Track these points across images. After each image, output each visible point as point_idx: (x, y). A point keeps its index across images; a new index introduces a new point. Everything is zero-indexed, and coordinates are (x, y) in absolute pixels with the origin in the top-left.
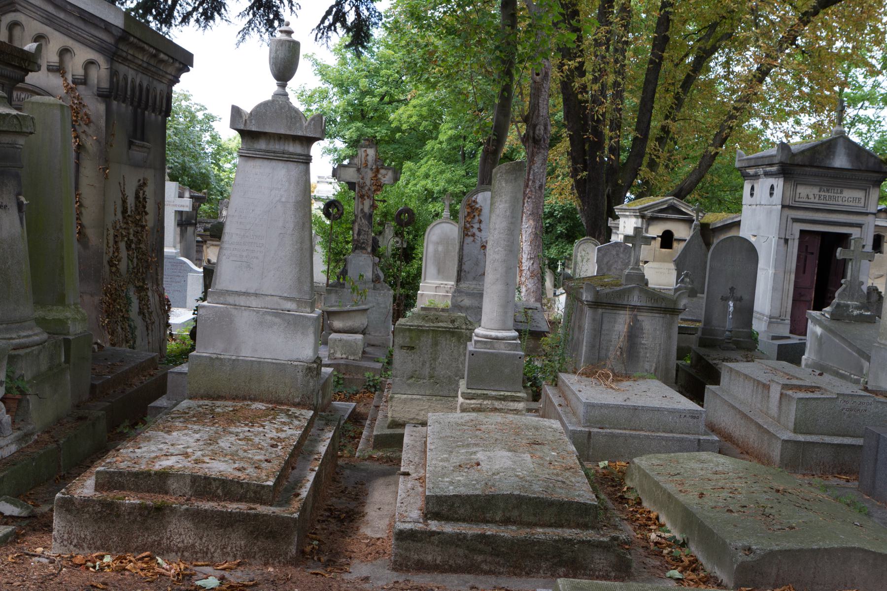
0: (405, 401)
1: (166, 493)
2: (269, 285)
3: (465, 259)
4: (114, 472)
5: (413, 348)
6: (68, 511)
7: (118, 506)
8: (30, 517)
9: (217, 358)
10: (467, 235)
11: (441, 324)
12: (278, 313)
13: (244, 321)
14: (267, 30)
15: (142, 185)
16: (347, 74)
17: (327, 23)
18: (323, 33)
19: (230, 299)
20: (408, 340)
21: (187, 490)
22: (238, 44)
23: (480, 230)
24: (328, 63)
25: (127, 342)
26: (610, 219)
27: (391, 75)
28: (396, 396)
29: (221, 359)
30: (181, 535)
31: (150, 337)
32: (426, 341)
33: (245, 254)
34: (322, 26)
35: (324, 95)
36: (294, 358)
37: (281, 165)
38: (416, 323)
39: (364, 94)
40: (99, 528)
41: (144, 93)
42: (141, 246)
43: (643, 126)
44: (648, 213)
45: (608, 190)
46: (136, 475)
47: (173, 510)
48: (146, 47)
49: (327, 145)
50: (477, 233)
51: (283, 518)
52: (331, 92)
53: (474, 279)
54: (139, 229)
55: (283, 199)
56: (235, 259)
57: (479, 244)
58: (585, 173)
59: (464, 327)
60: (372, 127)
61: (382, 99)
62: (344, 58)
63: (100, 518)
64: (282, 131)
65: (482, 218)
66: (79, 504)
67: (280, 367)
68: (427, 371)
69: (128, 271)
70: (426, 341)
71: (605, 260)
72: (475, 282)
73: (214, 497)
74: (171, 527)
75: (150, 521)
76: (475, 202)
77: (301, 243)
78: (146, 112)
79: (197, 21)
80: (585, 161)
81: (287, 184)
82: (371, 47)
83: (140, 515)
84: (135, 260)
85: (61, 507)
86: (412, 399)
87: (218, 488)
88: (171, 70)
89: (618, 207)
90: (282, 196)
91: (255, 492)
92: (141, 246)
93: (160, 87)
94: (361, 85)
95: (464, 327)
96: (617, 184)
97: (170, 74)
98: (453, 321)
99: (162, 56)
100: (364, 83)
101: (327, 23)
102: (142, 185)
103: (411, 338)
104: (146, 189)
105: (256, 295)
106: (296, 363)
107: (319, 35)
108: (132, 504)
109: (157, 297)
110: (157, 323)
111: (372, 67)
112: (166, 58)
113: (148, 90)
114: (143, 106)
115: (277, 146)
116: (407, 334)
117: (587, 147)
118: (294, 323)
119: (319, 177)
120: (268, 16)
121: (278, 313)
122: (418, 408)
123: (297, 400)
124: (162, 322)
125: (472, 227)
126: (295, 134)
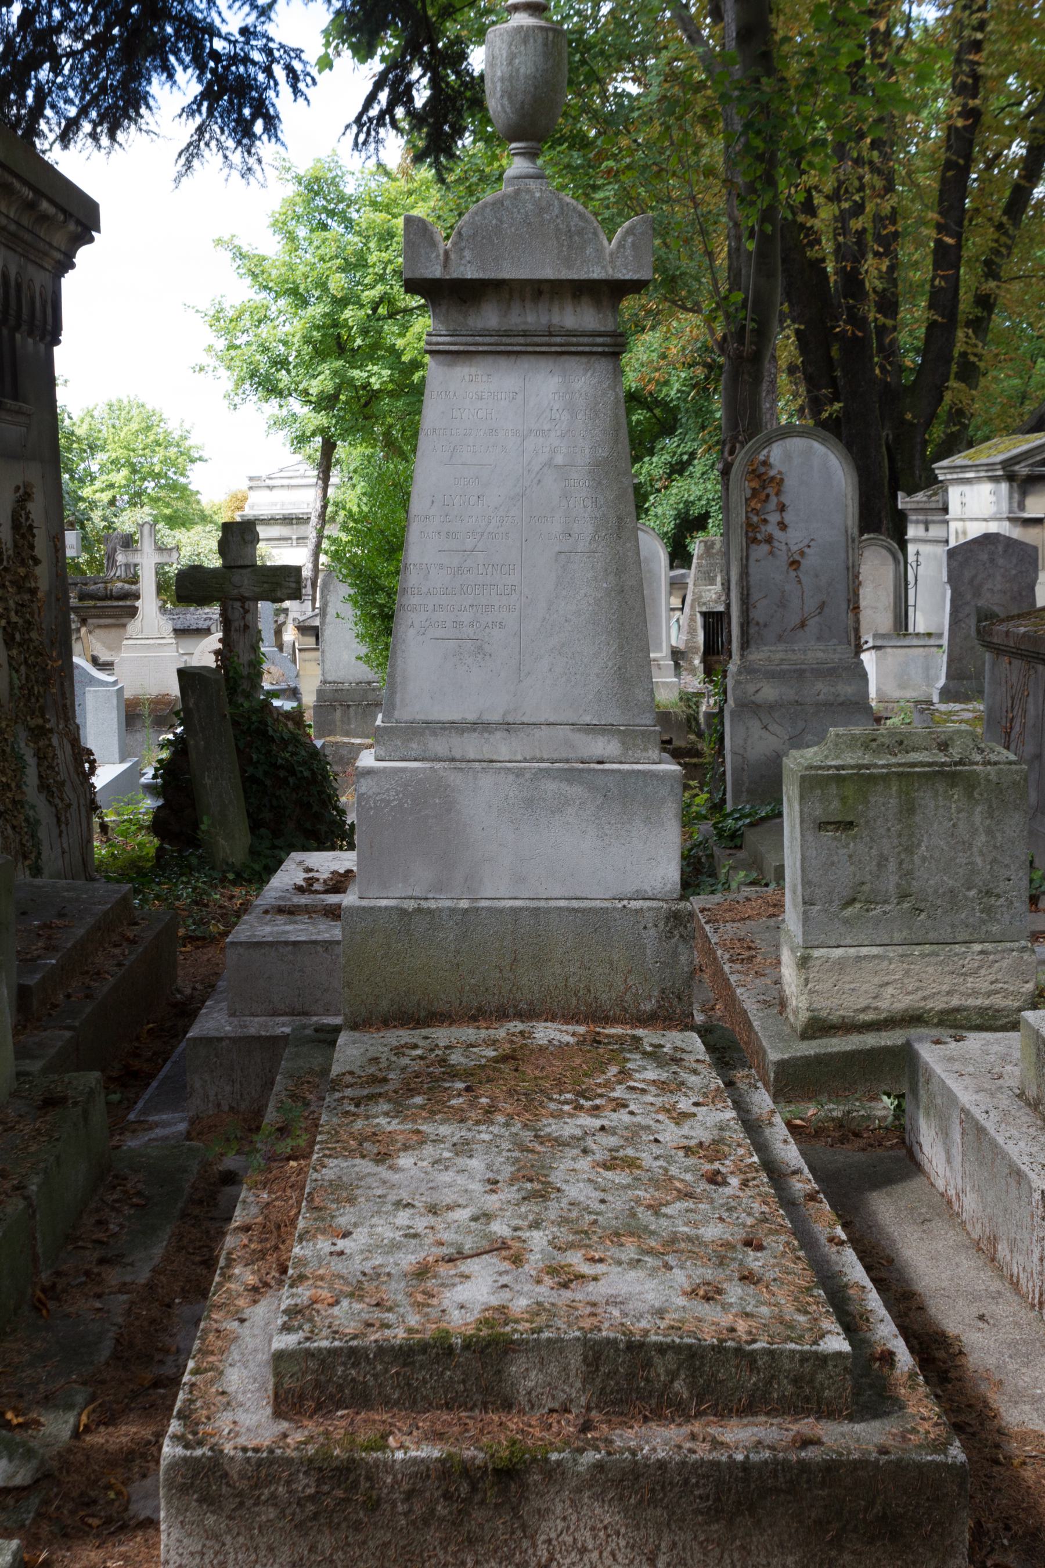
0: (841, 964)
1: (508, 1405)
2: (539, 700)
3: (755, 596)
4: (333, 1352)
5: (850, 825)
6: (209, 1501)
7: (372, 1472)
8: (37, 1481)
9: (419, 910)
10: (754, 540)
11: (914, 757)
12: (578, 773)
13: (483, 803)
14: (239, 143)
15: (24, 497)
16: (302, 269)
17: (374, 112)
18: (368, 134)
19: (439, 745)
20: (835, 804)
21: (574, 1390)
22: (177, 180)
23: (783, 526)
24: (262, 251)
25: (25, 857)
26: (900, 495)
27: (390, 262)
28: (816, 953)
29: (429, 911)
30: (583, 1550)
31: (64, 839)
32: (885, 803)
33: (466, 617)
34: (365, 118)
36: (630, 888)
37: (545, 365)
38: (850, 758)
39: (341, 303)
40: (312, 1549)
41: (13, 292)
42: (34, 635)
43: (943, 300)
44: (1022, 470)
45: (887, 433)
46: (405, 1355)
47: (553, 1473)
48: (17, 185)
50: (777, 534)
51: (920, 1466)
52: (274, 308)
53: (780, 638)
54: (27, 597)
55: (559, 460)
56: (440, 633)
57: (783, 559)
58: (837, 406)
59: (978, 758)
60: (360, 367)
61: (375, 310)
62: (291, 237)
63: (316, 1516)
64: (548, 273)
65: (785, 499)
66: (242, 1475)
67: (593, 922)
68: (891, 882)
69: (11, 695)
70: (885, 803)
71: (967, 575)
72: (781, 647)
73: (663, 1407)
74: (550, 1528)
75: (478, 1515)
76: (765, 463)
77: (618, 573)
78: (18, 336)
79: (94, 136)
80: (833, 382)
81: (565, 416)
83: (447, 1496)
84: (23, 669)
85: (184, 1489)
86: (859, 959)
87: (673, 1376)
88: (59, 239)
89: (945, 463)
91: (796, 1381)
92: (34, 635)
93: (40, 278)
94: (331, 285)
95: (978, 758)
96: (903, 422)
97: (58, 250)
98: (944, 746)
99: (45, 205)
100: (338, 283)
101: (374, 112)
102: (24, 497)
103: (843, 799)
104: (30, 506)
105: (508, 726)
106: (635, 905)
107: (362, 137)
108: (415, 1461)
109: (68, 748)
110: (75, 806)
111: (350, 249)
112: (51, 210)
113: (19, 286)
114: (12, 321)
115: (531, 317)
116: (833, 789)
117: (835, 352)
118: (622, 795)
119: (251, 479)
120: (240, 113)
121: (578, 773)
122: (876, 980)
123: (648, 1006)
124: (82, 801)
125: (765, 521)
126: (583, 276)
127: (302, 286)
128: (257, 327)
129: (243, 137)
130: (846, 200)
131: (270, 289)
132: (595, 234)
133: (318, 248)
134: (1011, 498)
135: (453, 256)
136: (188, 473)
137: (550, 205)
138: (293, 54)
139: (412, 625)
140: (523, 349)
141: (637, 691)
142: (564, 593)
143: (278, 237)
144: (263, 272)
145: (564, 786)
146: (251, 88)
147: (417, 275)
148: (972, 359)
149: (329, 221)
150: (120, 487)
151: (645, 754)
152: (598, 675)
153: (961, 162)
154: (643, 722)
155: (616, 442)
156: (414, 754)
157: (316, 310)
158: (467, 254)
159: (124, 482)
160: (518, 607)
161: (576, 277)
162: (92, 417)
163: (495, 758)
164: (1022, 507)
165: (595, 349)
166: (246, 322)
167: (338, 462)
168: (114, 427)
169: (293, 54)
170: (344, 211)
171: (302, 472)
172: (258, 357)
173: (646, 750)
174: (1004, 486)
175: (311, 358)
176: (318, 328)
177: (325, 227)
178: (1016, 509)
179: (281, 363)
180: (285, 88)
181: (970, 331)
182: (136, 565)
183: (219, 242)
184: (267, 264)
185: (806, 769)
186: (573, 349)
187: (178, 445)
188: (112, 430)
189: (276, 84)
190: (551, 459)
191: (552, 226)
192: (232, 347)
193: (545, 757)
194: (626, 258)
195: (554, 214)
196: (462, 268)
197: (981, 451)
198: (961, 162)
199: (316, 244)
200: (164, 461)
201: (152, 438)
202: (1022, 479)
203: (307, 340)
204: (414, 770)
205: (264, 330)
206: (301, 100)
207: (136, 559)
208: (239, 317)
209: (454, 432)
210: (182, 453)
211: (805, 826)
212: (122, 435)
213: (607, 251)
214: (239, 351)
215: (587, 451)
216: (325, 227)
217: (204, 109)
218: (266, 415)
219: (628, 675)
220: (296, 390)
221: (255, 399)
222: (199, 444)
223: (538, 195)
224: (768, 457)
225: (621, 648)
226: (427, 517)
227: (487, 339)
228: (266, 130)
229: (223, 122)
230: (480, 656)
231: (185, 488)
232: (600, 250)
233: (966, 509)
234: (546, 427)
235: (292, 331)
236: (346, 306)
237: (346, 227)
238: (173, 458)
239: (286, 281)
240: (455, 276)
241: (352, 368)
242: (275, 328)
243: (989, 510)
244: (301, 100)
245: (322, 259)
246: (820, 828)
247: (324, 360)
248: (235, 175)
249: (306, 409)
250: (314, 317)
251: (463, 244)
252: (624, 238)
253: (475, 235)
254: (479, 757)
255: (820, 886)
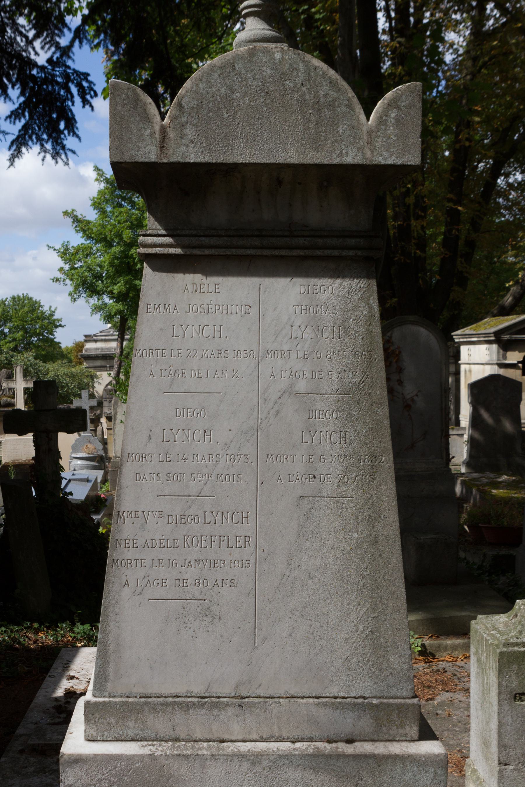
16: (109, 227)
24: (88, 218)
33: (191, 573)
35: (88, 253)
49: (96, 302)
52: (94, 248)
55: (302, 386)
56: (160, 592)
77: (372, 521)
82: (131, 198)
89: (459, 332)
90: (295, 375)
94: (124, 236)
100: (127, 234)
105: (241, 701)
119: (86, 336)
126: (335, 160)
127: (109, 236)
128: (86, 258)
129: (53, 132)
130: (403, 187)
131: (93, 238)
132: (350, 106)
133: (117, 216)
134: (498, 352)
135: (171, 134)
136: (55, 333)
137: (293, 69)
138: (82, 77)
139: (127, 583)
140: (258, 252)
141: (392, 658)
142: (307, 544)
143: (96, 211)
144: (89, 229)
145: (309, 775)
146: (57, 100)
147: (127, 158)
148: (466, 275)
149: (123, 203)
150: (19, 340)
151: (401, 731)
152: (347, 640)
153: (461, 168)
154: (398, 694)
155: (370, 365)
156: (130, 734)
157: (116, 249)
158: (190, 131)
159: (21, 338)
160: (252, 562)
161: (326, 161)
162: (5, 304)
163: (226, 737)
164: (505, 357)
165: (345, 253)
166: (80, 255)
167: (129, 328)
168: (15, 309)
169: (82, 77)
170: (131, 198)
171: (111, 332)
172: (86, 274)
173: (402, 726)
174: (495, 347)
175: (114, 274)
176: (117, 258)
177: (121, 206)
178: (501, 359)
179: (98, 277)
180: (77, 100)
181: (463, 260)
182: (14, 389)
183: (66, 213)
184: (91, 226)
185: (504, 645)
186: (319, 253)
187: (49, 319)
188: (15, 311)
189: (72, 96)
190: (292, 385)
191: (296, 96)
192: (73, 268)
193: (285, 735)
194: (389, 138)
195: (299, 81)
196: (183, 149)
197: (480, 326)
198: (461, 168)
199: (116, 214)
200: (41, 327)
201: (35, 315)
202: (504, 341)
203: (111, 264)
204: (130, 759)
205: (89, 260)
206: (87, 107)
207: (13, 385)
208: (77, 253)
209: (175, 353)
210: (51, 323)
211: (503, 696)
212: (20, 313)
213: (365, 129)
214: (77, 271)
215: (335, 375)
216: (121, 206)
217: (27, 114)
218: (91, 305)
219: (382, 640)
220: (106, 291)
221: (85, 295)
222: (59, 318)
223: (278, 56)
224: (391, 337)
225: (374, 608)
226: (143, 456)
227: (214, 241)
228: (66, 127)
229: (40, 122)
230: (208, 619)
231: (52, 340)
232: (355, 127)
233: (471, 358)
234: (286, 348)
235: (104, 260)
236: (132, 247)
237: (132, 206)
238: (46, 325)
239: (101, 234)
240: (174, 159)
241: (135, 279)
242: (95, 258)
243: (485, 358)
244: (87, 107)
245: (119, 222)
246: (515, 697)
247: (120, 276)
248: (49, 157)
249: (111, 301)
250: (115, 252)
251: (184, 119)
252: (385, 112)
253: (199, 106)
254: (207, 736)
255: (515, 749)
